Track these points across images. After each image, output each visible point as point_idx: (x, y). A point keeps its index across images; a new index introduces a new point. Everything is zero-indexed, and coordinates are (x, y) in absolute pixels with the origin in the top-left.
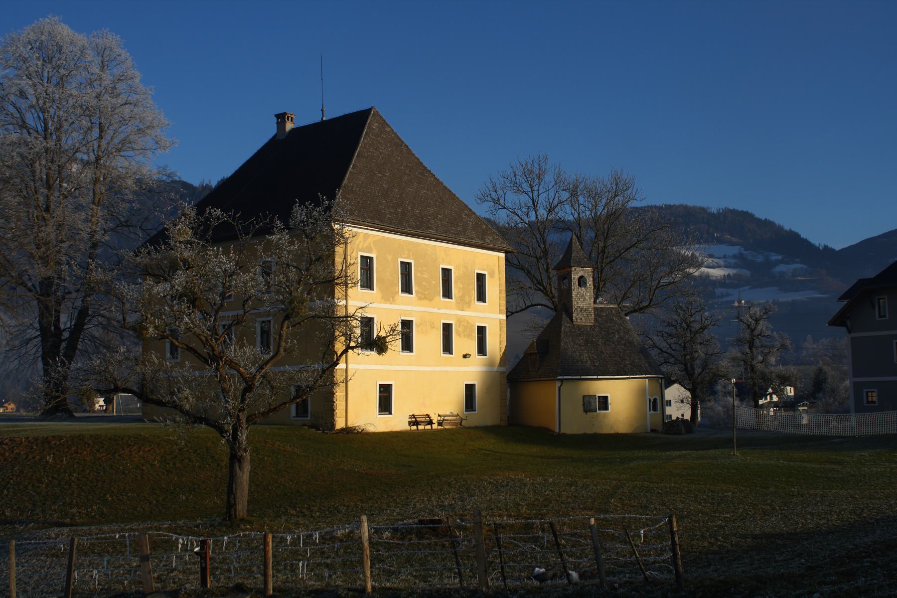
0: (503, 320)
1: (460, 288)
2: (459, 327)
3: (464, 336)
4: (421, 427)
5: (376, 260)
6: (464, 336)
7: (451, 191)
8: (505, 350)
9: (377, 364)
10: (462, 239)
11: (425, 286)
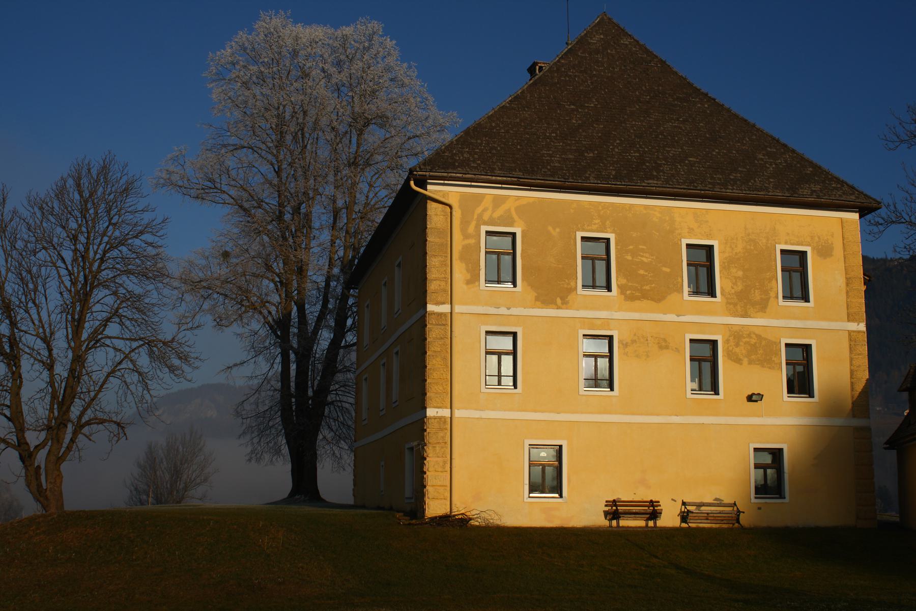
0: (429, 304)
1: (736, 278)
2: (737, 345)
3: (750, 363)
4: (624, 523)
5: (617, 244)
6: (750, 363)
7: (746, 121)
8: (865, 387)
9: (535, 411)
10: (729, 192)
11: (643, 276)
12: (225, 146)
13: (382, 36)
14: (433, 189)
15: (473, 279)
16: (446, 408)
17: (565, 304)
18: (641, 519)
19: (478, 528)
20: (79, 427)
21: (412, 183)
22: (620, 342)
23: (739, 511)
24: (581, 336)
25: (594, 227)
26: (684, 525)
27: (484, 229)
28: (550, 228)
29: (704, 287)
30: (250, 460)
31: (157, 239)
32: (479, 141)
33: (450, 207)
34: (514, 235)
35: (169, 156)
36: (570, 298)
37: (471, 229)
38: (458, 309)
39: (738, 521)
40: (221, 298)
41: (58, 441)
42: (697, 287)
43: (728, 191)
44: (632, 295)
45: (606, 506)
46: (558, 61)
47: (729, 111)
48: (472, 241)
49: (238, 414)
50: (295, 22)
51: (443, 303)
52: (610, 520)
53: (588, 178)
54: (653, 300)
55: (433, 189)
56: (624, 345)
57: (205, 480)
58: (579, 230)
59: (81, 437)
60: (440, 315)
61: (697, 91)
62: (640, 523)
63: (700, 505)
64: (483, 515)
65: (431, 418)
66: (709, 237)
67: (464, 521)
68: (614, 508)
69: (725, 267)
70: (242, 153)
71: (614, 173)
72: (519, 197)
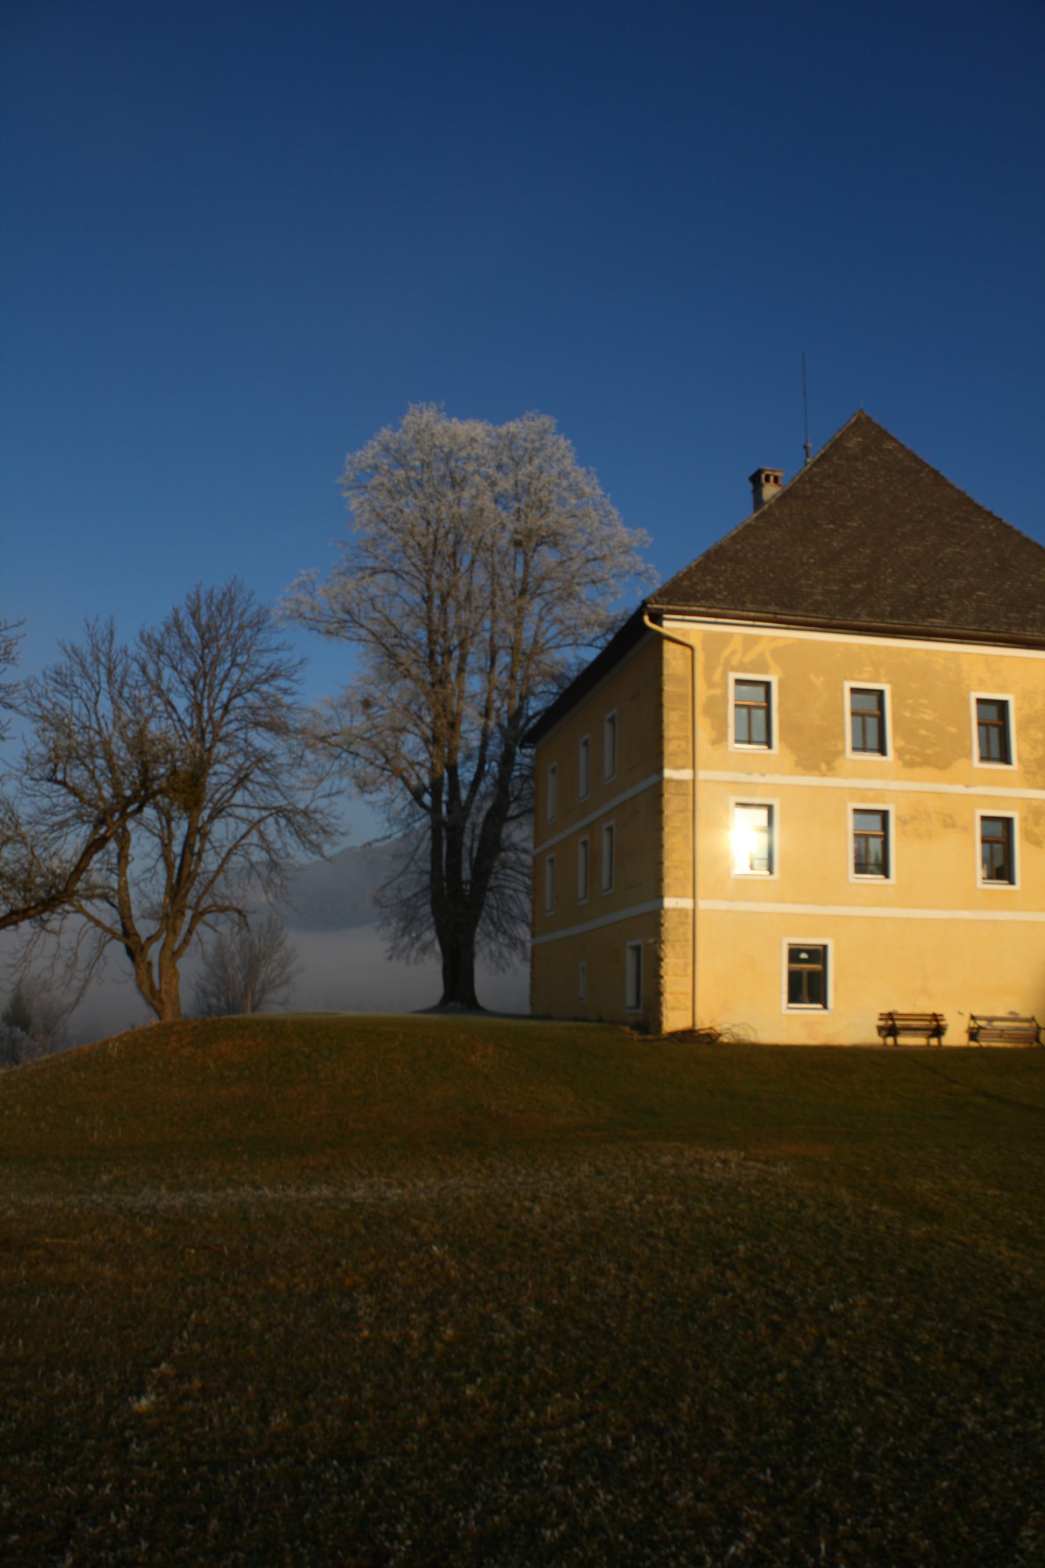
5: (893, 697)
10: (1029, 634)
12: (361, 569)
13: (554, 434)
14: (670, 626)
15: (720, 738)
16: (688, 897)
17: (831, 770)
18: (922, 1035)
19: (728, 1045)
20: (198, 916)
21: (646, 619)
22: (898, 818)
23: (1039, 1029)
24: (732, 805)
25: (866, 676)
26: (973, 1044)
27: (733, 676)
28: (812, 677)
29: (995, 752)
30: (390, 958)
31: (293, 684)
32: (723, 567)
33: (692, 648)
34: (767, 685)
35: (296, 581)
36: (837, 763)
37: (717, 677)
38: (702, 775)
39: (1037, 1039)
40: (350, 758)
41: (174, 931)
42: (989, 751)
43: (1027, 633)
44: (914, 760)
45: (881, 1019)
46: (810, 469)
47: (1018, 534)
48: (718, 691)
49: (377, 901)
50: (450, 417)
51: (683, 767)
52: (885, 1037)
53: (858, 616)
54: (936, 766)
55: (670, 626)
56: (902, 822)
57: (287, 981)
58: (847, 679)
59: (200, 927)
60: (680, 783)
61: (979, 509)
62: (918, 1041)
63: (991, 1020)
64: (735, 1030)
65: (669, 910)
66: (1003, 689)
67: (710, 1039)
68: (890, 1022)
69: (1022, 728)
70: (380, 578)
71: (888, 609)
72: (774, 639)
